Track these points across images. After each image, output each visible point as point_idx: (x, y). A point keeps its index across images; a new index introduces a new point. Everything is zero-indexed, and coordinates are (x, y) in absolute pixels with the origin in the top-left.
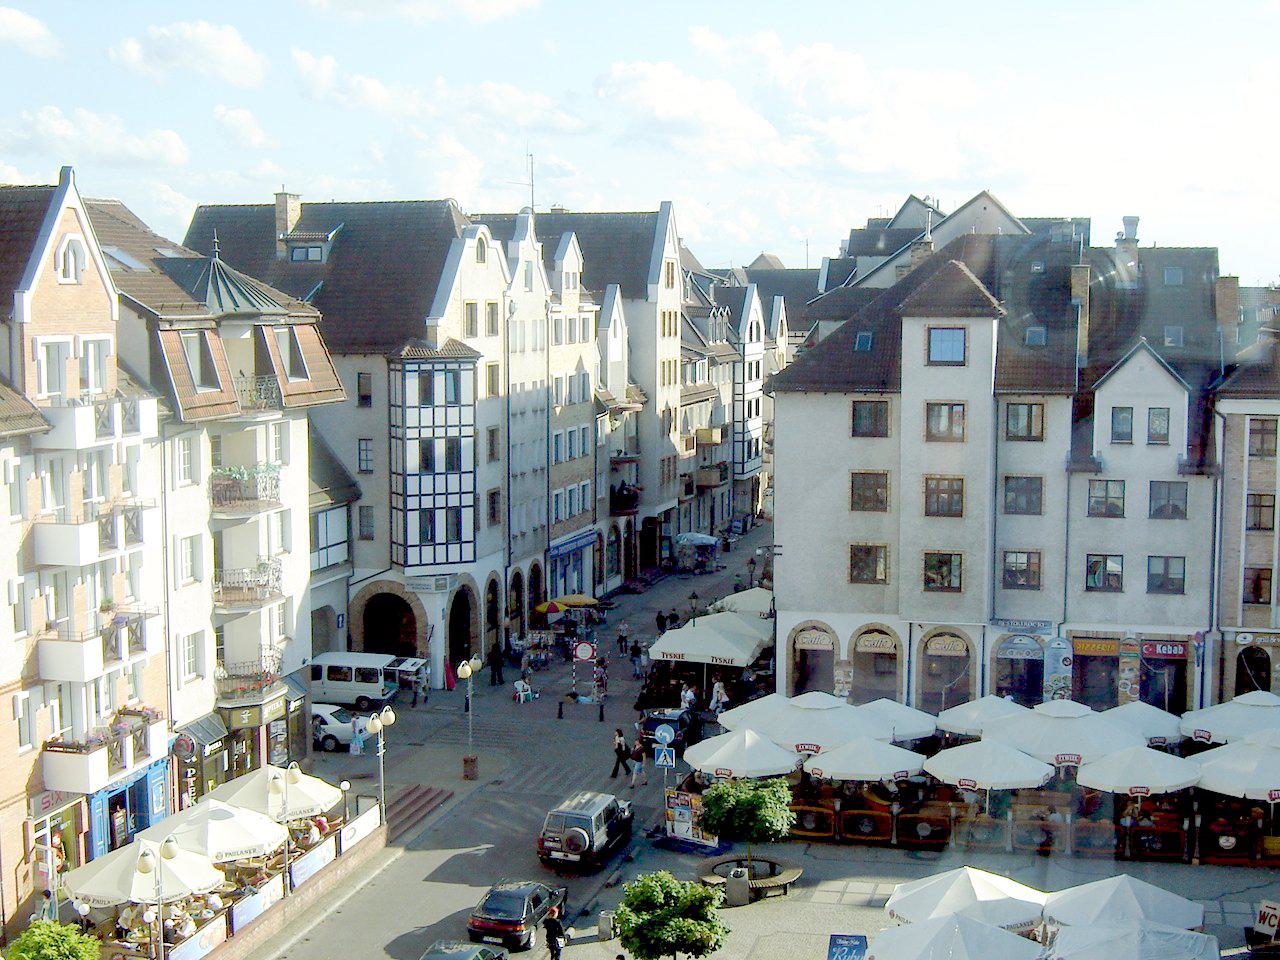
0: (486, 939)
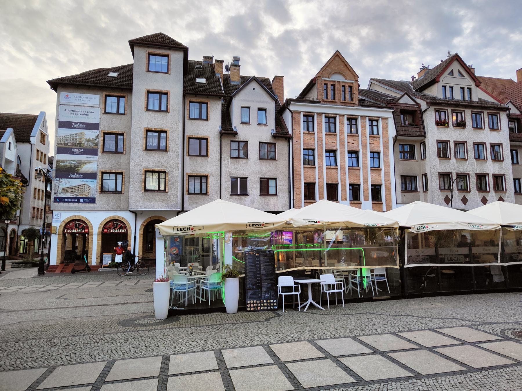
0: (452, 272)
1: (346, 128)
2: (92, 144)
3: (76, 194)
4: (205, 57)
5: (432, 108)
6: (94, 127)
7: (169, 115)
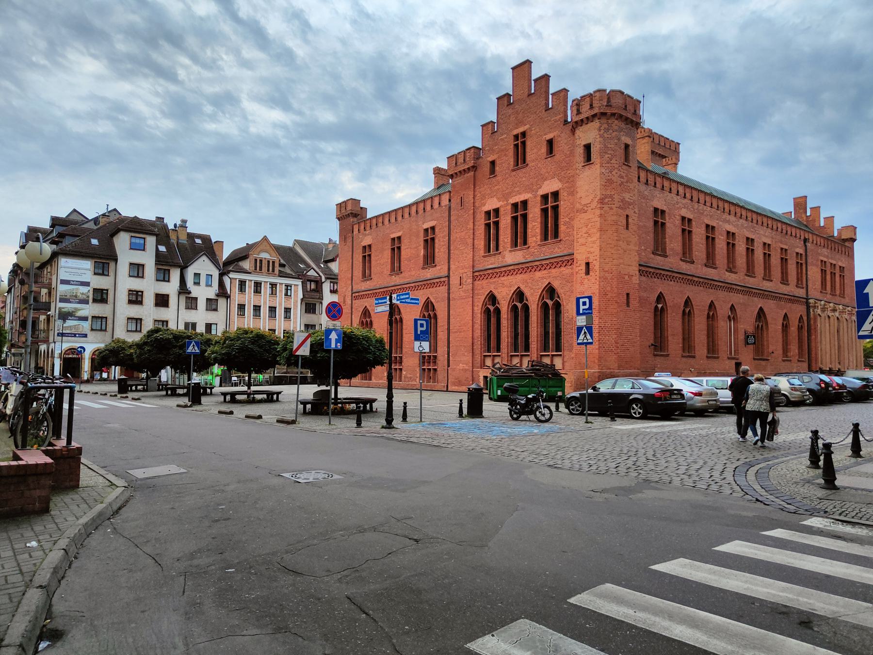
1: (269, 291)
2: (85, 297)
3: (73, 331)
4: (157, 218)
5: (329, 281)
6: (87, 284)
7: (145, 280)
